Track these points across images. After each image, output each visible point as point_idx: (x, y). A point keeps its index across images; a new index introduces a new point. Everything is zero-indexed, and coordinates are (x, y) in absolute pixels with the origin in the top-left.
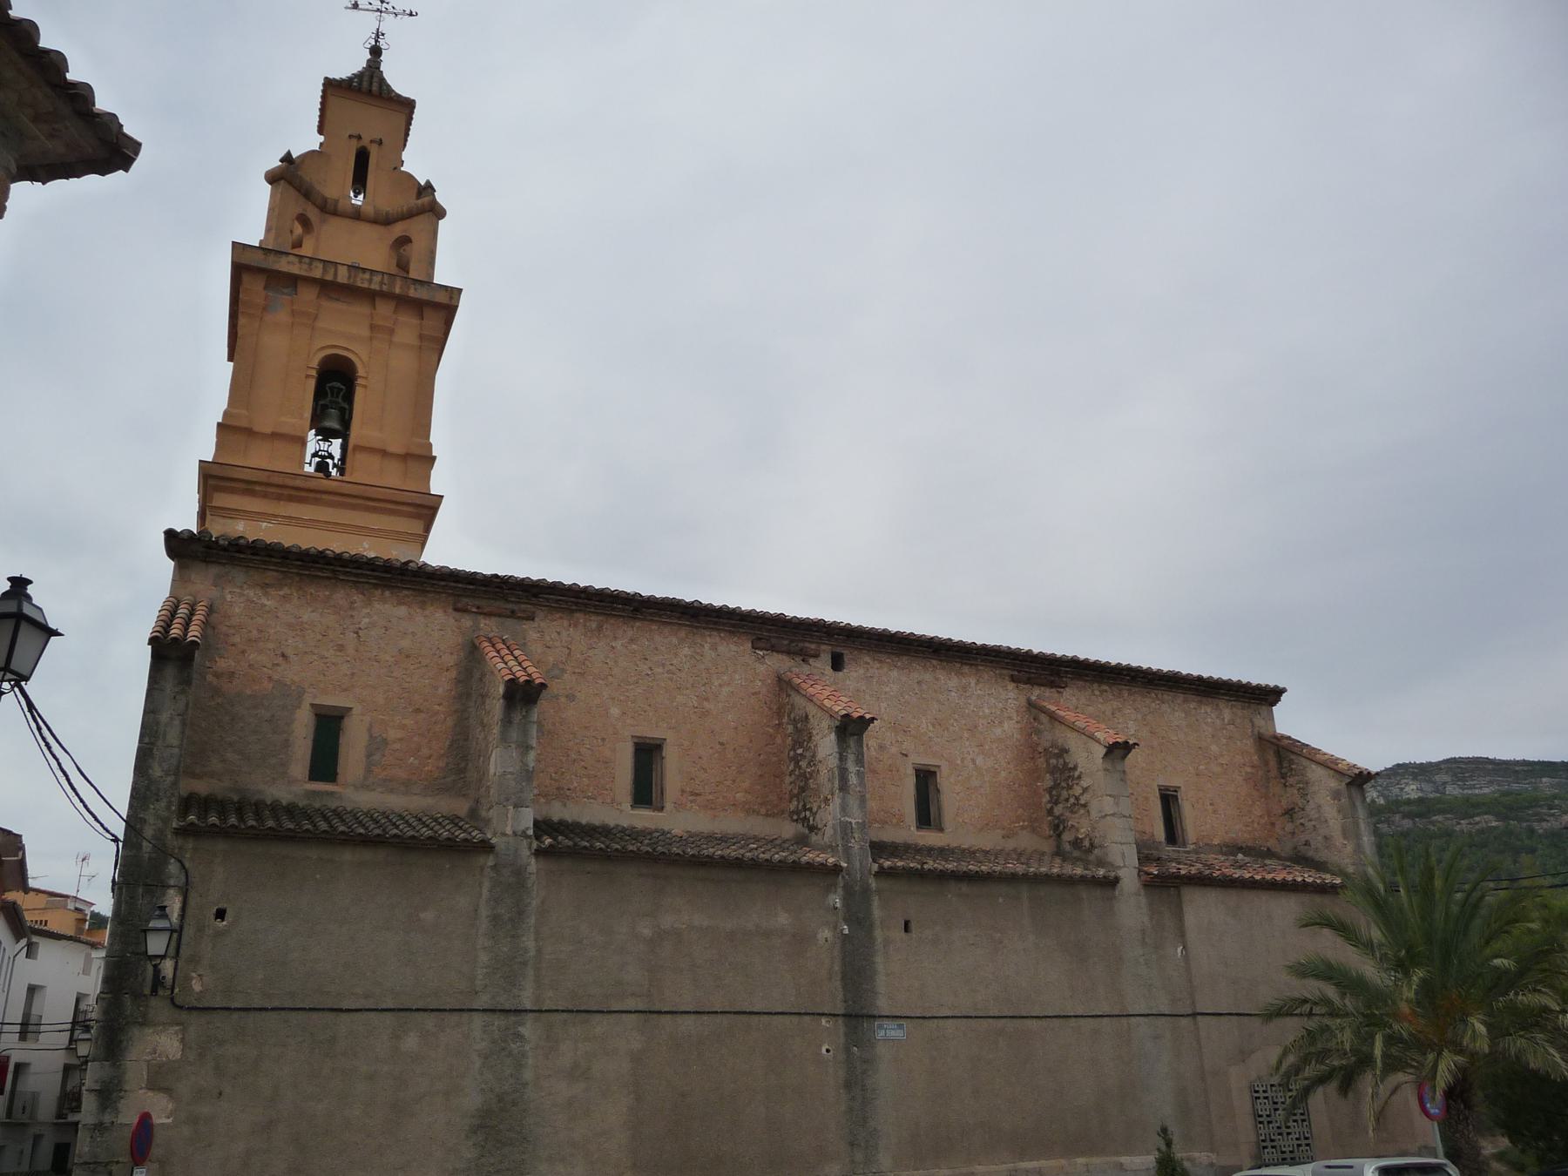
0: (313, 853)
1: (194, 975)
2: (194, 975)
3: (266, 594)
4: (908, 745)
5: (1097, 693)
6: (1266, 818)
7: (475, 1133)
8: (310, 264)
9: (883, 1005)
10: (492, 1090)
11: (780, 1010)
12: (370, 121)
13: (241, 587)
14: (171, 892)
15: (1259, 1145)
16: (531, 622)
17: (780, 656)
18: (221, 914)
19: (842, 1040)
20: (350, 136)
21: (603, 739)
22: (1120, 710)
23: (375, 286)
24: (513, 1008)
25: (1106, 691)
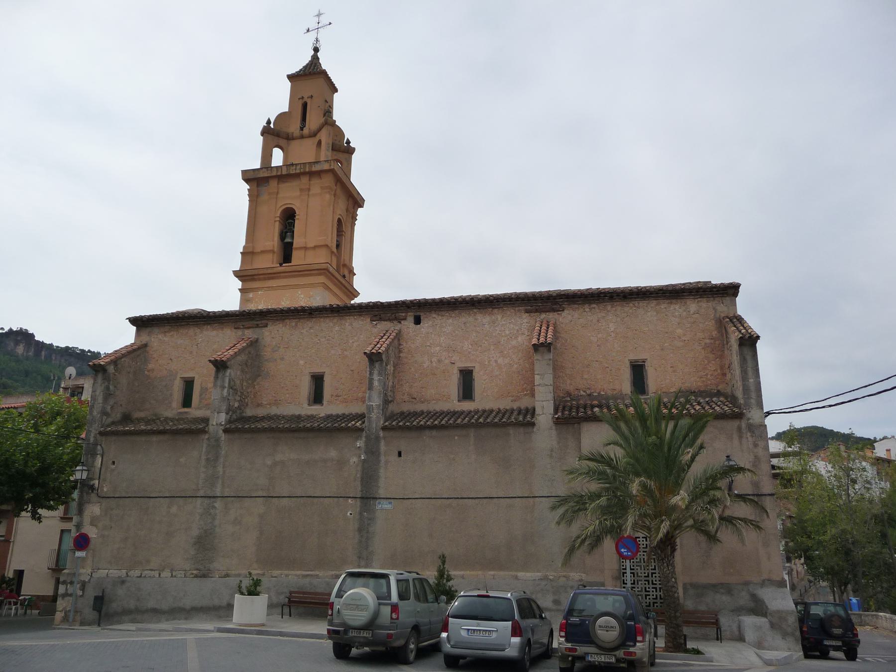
0: (143, 439)
1: (104, 485)
2: (104, 485)
3: (165, 335)
4: (455, 358)
5: (587, 310)
6: (719, 371)
7: (195, 544)
8: (271, 170)
9: (382, 493)
10: (202, 528)
11: (328, 496)
12: (311, 87)
13: (157, 335)
14: (98, 456)
15: (621, 571)
16: (266, 328)
17: (386, 323)
18: (114, 463)
19: (358, 509)
20: (299, 99)
21: (296, 376)
22: (604, 317)
23: (298, 171)
24: (212, 496)
25: (594, 308)
